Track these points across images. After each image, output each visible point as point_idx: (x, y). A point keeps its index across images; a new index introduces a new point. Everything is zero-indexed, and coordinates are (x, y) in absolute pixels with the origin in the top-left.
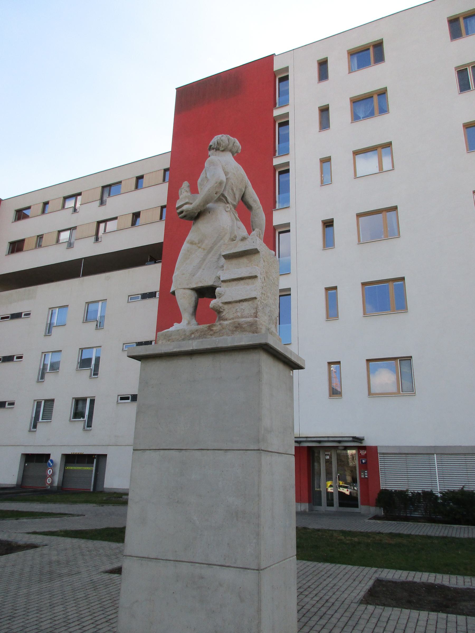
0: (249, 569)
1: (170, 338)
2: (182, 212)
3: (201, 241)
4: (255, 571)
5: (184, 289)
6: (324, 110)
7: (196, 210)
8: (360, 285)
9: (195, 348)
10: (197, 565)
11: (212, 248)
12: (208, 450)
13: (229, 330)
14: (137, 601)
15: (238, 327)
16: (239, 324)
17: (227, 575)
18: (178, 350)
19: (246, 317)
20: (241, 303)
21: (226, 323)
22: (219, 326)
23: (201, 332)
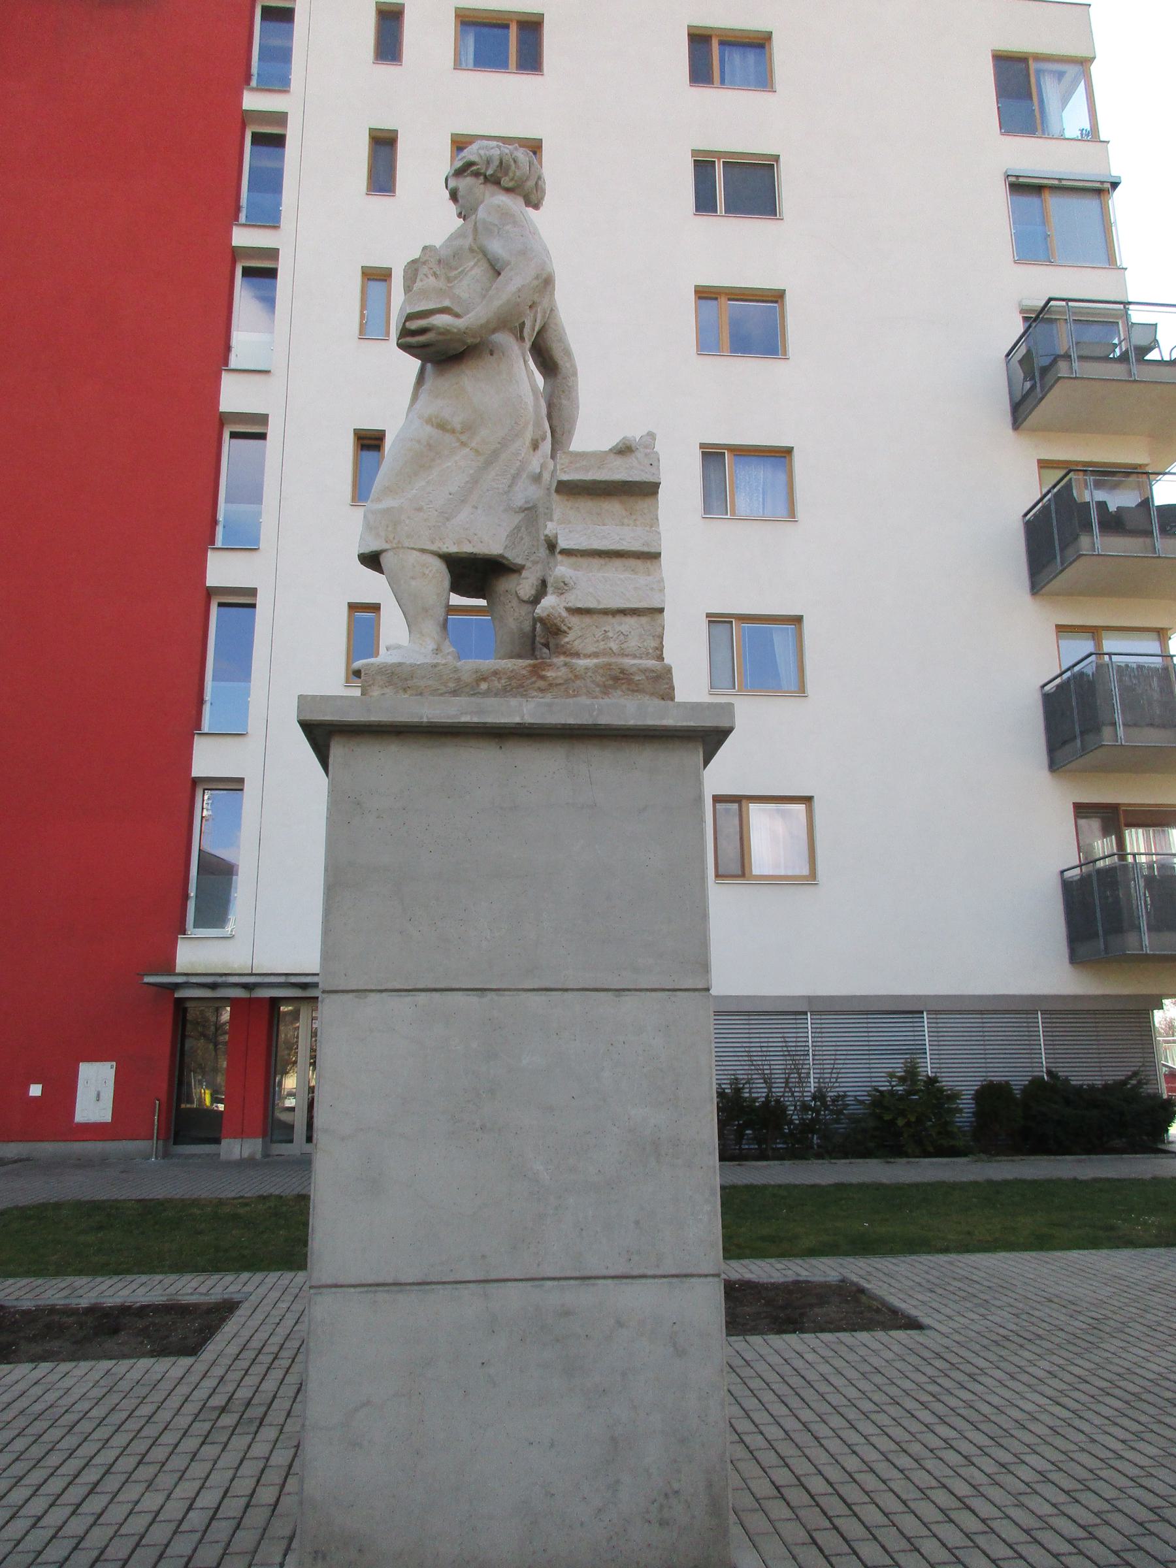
0: (692, 1276)
1: (410, 683)
2: (423, 331)
3: (469, 428)
4: (710, 1279)
5: (423, 551)
6: (383, 144)
7: (474, 337)
8: (345, 609)
9: (529, 719)
10: (549, 1283)
11: (495, 454)
12: (566, 990)
13: (593, 682)
14: (368, 1403)
15: (619, 679)
16: (623, 671)
17: (637, 1298)
18: (476, 720)
19: (635, 657)
20: (619, 618)
21: (582, 663)
22: (564, 669)
23: (510, 678)
